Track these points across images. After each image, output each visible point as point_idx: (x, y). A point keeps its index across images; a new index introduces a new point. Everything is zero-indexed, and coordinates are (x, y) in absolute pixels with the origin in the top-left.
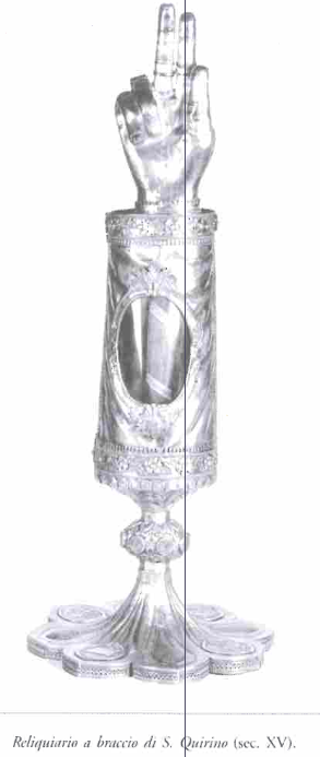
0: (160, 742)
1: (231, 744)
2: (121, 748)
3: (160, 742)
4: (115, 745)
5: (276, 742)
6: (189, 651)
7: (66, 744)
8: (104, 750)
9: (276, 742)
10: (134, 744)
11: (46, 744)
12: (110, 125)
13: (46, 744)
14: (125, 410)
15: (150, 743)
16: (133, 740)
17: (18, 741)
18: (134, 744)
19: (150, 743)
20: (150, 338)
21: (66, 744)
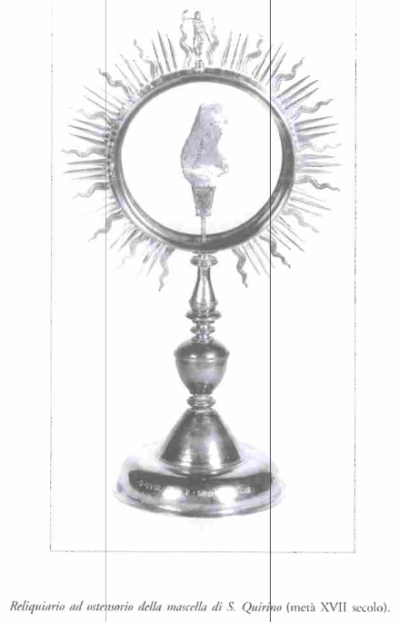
0: (225, 606)
1: (284, 608)
2: (189, 611)
3: (225, 606)
4: (33, 608)
5: (329, 607)
6: (278, 255)
7: (124, 608)
8: (172, 612)
9: (329, 607)
10: (131, 608)
11: (38, 607)
12: (181, 12)
13: (38, 607)
14: (200, 173)
15: (217, 608)
16: (129, 605)
17: (14, 606)
18: (131, 608)
19: (217, 608)
20: (262, 101)
21: (124, 608)
